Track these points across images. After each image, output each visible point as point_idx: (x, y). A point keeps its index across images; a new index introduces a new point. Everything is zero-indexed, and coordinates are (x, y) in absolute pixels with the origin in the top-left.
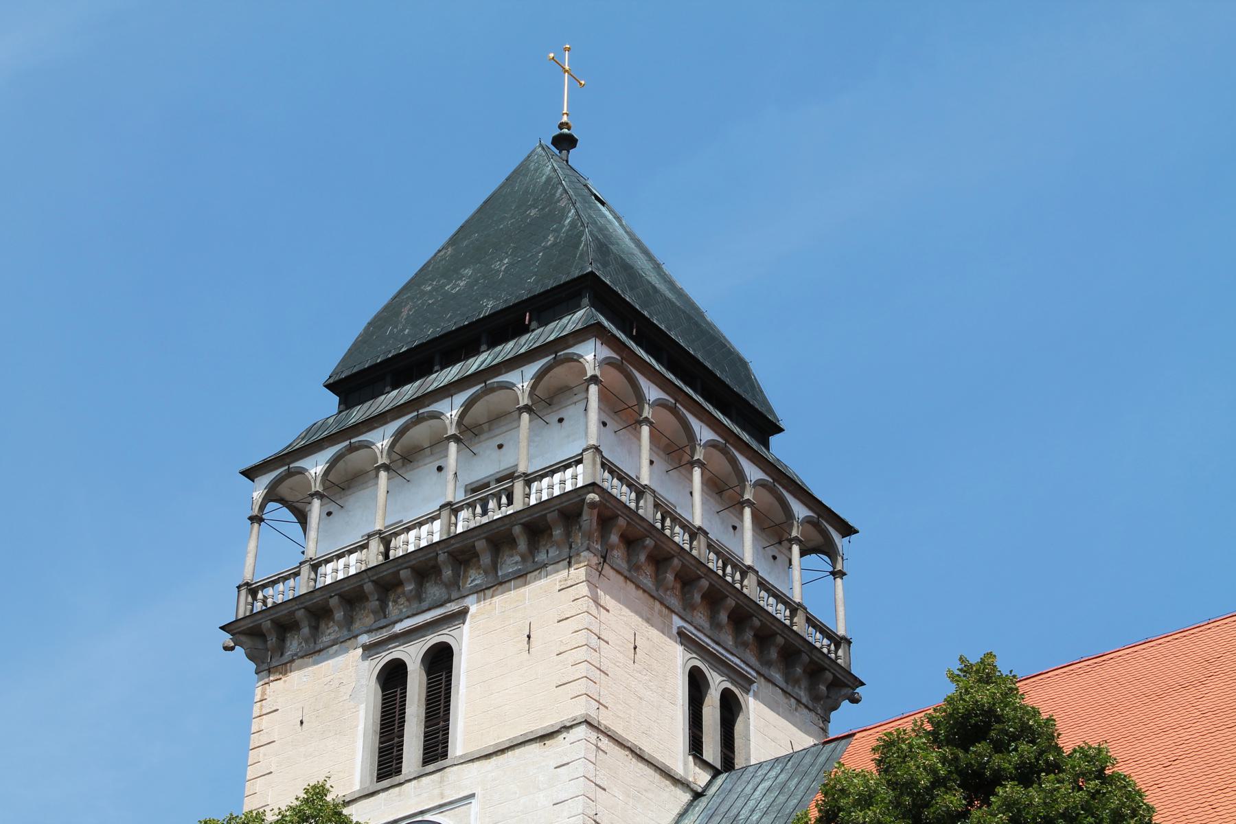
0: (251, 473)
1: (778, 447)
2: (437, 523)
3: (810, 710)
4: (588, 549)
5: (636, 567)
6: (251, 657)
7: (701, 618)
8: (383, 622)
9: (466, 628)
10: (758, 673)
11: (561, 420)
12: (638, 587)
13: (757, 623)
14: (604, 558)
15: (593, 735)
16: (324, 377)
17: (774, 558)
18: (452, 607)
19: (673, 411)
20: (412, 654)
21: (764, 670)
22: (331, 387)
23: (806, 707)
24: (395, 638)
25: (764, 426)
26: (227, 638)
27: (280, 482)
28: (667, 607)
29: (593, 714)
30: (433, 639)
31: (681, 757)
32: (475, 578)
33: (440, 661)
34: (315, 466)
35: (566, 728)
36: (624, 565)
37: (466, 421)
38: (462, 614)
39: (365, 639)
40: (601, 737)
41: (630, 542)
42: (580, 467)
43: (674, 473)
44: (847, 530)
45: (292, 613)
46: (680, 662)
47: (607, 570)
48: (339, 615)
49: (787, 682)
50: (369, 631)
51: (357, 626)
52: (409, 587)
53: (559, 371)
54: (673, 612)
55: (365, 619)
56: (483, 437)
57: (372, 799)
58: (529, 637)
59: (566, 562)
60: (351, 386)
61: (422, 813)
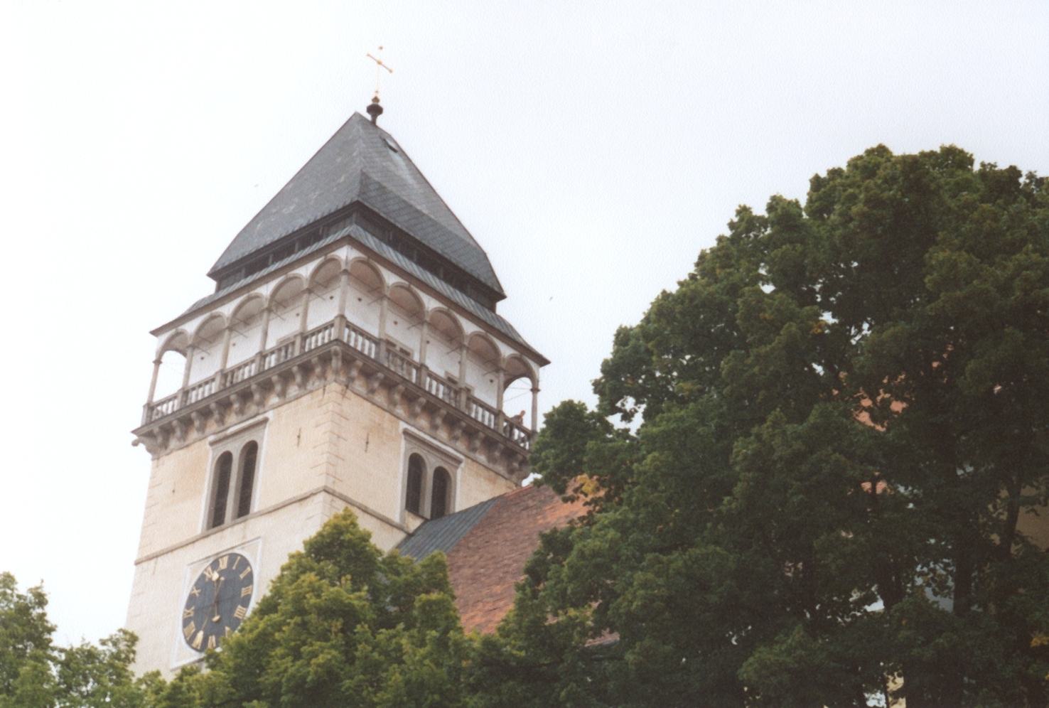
0: (155, 333)
1: (502, 308)
2: (253, 366)
3: (506, 479)
4: (335, 381)
5: (372, 391)
6: (149, 450)
7: (423, 422)
8: (222, 428)
9: (267, 430)
10: (466, 456)
11: (332, 298)
12: (374, 404)
13: (463, 424)
14: (347, 387)
15: (329, 497)
16: (208, 269)
17: (492, 381)
18: (260, 418)
19: (409, 289)
20: (236, 448)
21: (471, 455)
22: (213, 274)
23: (503, 477)
24: (227, 437)
25: (491, 293)
26: (135, 437)
27: (173, 337)
28: (395, 416)
29: (330, 486)
30: (247, 438)
31: (398, 511)
32: (274, 400)
33: (251, 450)
34: (191, 327)
35: (313, 494)
36: (363, 390)
37: (278, 297)
38: (266, 421)
39: (212, 438)
40: (335, 498)
41: (367, 374)
42: (333, 330)
43: (413, 329)
44: (543, 362)
45: (170, 423)
46: (403, 450)
47: (349, 393)
48: (197, 423)
49: (489, 462)
50: (214, 434)
51: (208, 430)
52: (236, 406)
53: (330, 266)
54: (401, 419)
55: (212, 426)
56: (288, 309)
57: (206, 539)
58: (299, 437)
59: (321, 390)
60: (221, 274)
61: (233, 548)
